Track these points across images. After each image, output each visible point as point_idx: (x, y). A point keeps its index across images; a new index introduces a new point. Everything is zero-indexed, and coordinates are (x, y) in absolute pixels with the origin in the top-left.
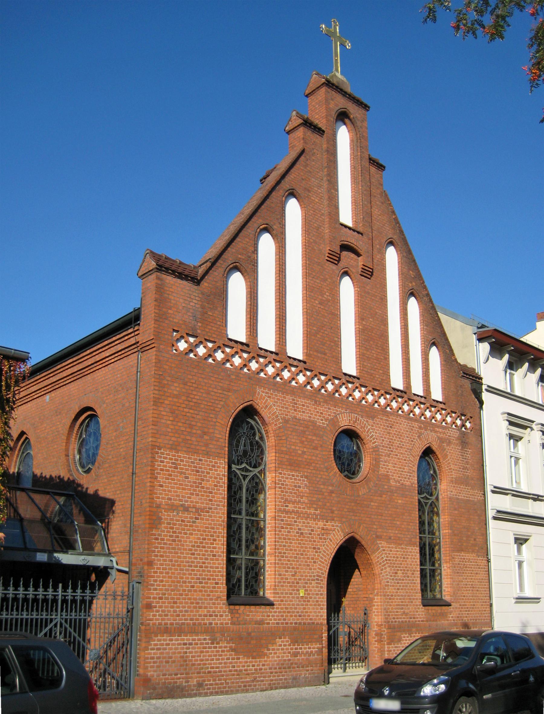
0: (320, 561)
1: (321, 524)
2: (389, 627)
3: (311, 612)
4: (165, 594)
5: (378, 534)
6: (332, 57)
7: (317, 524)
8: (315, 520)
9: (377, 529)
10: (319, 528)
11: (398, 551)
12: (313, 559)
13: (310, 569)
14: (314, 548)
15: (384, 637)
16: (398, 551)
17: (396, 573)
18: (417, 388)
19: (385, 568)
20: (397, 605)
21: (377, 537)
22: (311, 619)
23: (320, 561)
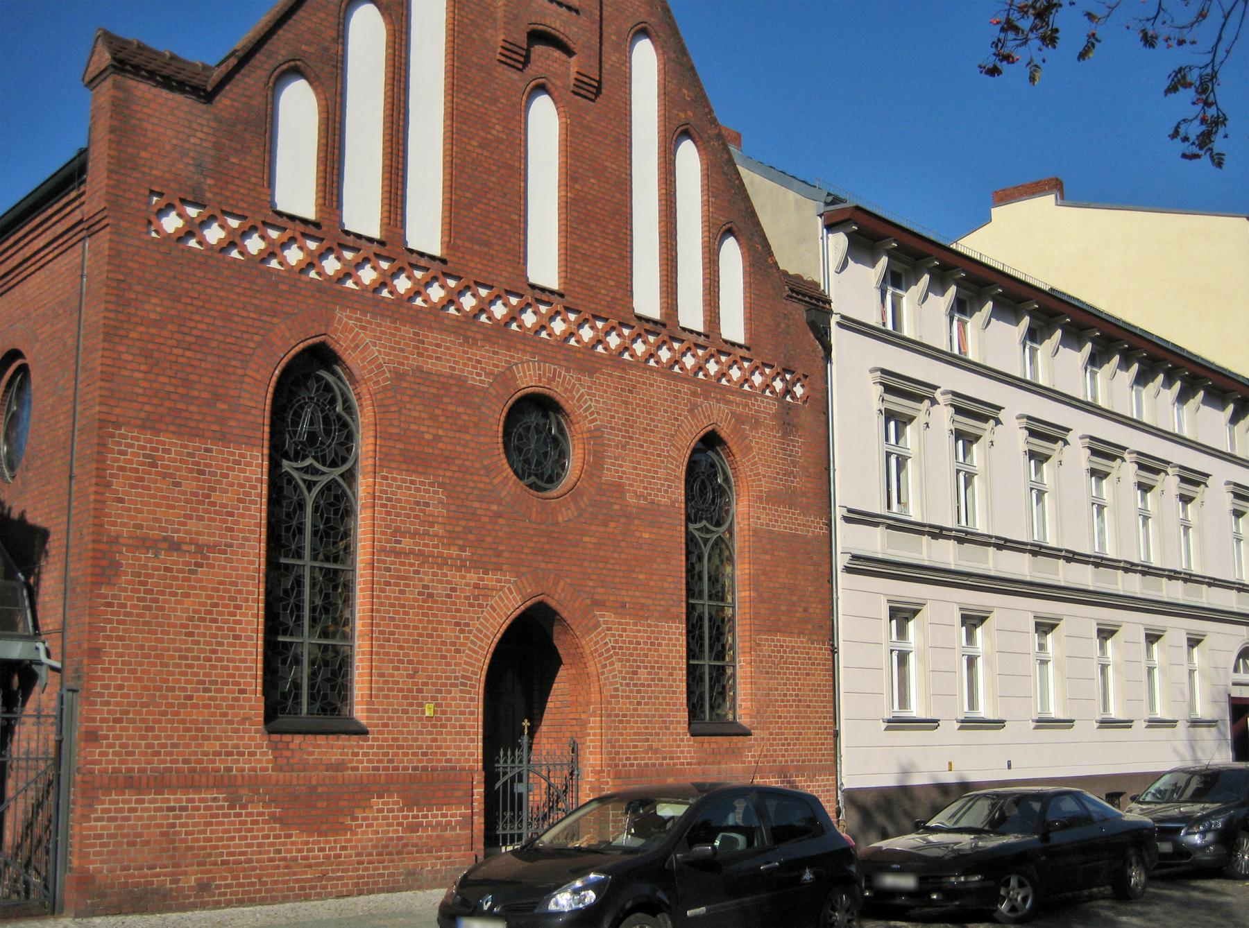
0: (470, 649)
1: (472, 577)
3: (448, 747)
5: (597, 597)
7: (463, 577)
8: (459, 569)
9: (594, 587)
10: (468, 585)
12: (453, 644)
16: (639, 631)
17: (635, 673)
19: (612, 664)
21: (595, 603)
22: (448, 761)
23: (470, 649)
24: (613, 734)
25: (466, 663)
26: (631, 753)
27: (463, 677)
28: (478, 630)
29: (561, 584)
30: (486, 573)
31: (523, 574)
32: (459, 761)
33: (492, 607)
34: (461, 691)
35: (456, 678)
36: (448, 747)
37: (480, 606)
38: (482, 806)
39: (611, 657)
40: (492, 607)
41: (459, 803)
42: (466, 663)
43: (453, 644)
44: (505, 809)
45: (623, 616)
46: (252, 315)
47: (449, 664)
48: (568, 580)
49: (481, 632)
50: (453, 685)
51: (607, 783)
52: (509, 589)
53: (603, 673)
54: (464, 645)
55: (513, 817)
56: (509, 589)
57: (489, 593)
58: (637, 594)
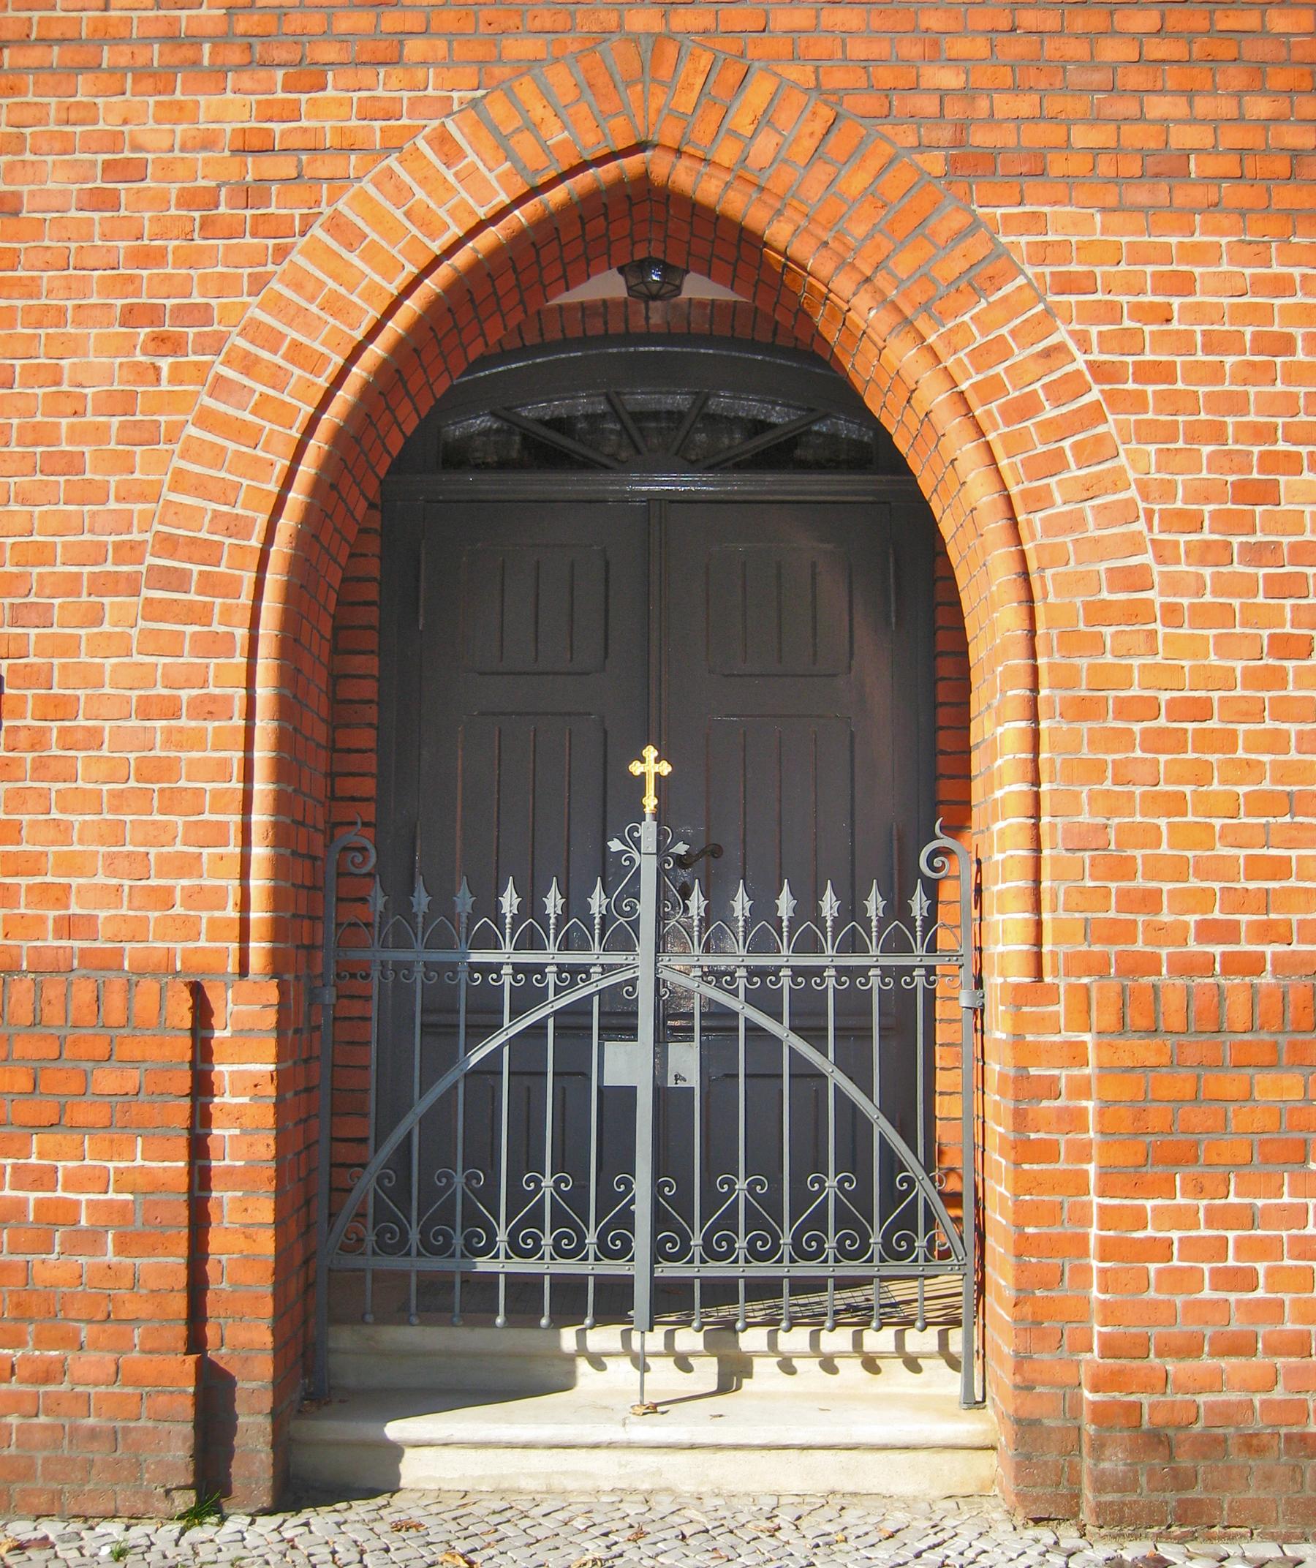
0: (206, 419)
1: (229, 109)
2: (1135, 1014)
3: (71, 865)
4: (1256, 678)
5: (980, 138)
6: (1058, 514)
7: (180, 112)
8: (160, 80)
9: (968, 93)
10: (208, 142)
11: (1282, 286)
12: (124, 403)
13: (96, 494)
14: (131, 316)
15: (1075, 1119)
16: (1282, 286)
17: (1267, 493)
18: (926, 1289)
19: (1096, 451)
20: (1261, 803)
21: (971, 165)
22: (68, 927)
23: (206, 419)
24: (1115, 804)
25: (180, 481)
26: (1239, 901)
27: (168, 544)
28: (255, 331)
29: (759, 92)
30: (309, 77)
31: (527, 67)
32: (137, 930)
33: (337, 226)
34: (153, 610)
35: (130, 551)
36: (71, 865)
37: (278, 228)
38: (265, 1146)
39: (1095, 414)
40: (337, 226)
41: (119, 1123)
42: (180, 481)
43: (124, 403)
44: (526, 1159)
45: (1182, 217)
46: (998, 1032)
47: (96, 494)
48: (799, 74)
49: (272, 340)
50: (105, 584)
51: (1076, 1054)
52: (443, 141)
53: (1039, 499)
54: (171, 402)
55: (577, 1199)
56: (443, 141)
57: (324, 167)
58: (1259, 107)
